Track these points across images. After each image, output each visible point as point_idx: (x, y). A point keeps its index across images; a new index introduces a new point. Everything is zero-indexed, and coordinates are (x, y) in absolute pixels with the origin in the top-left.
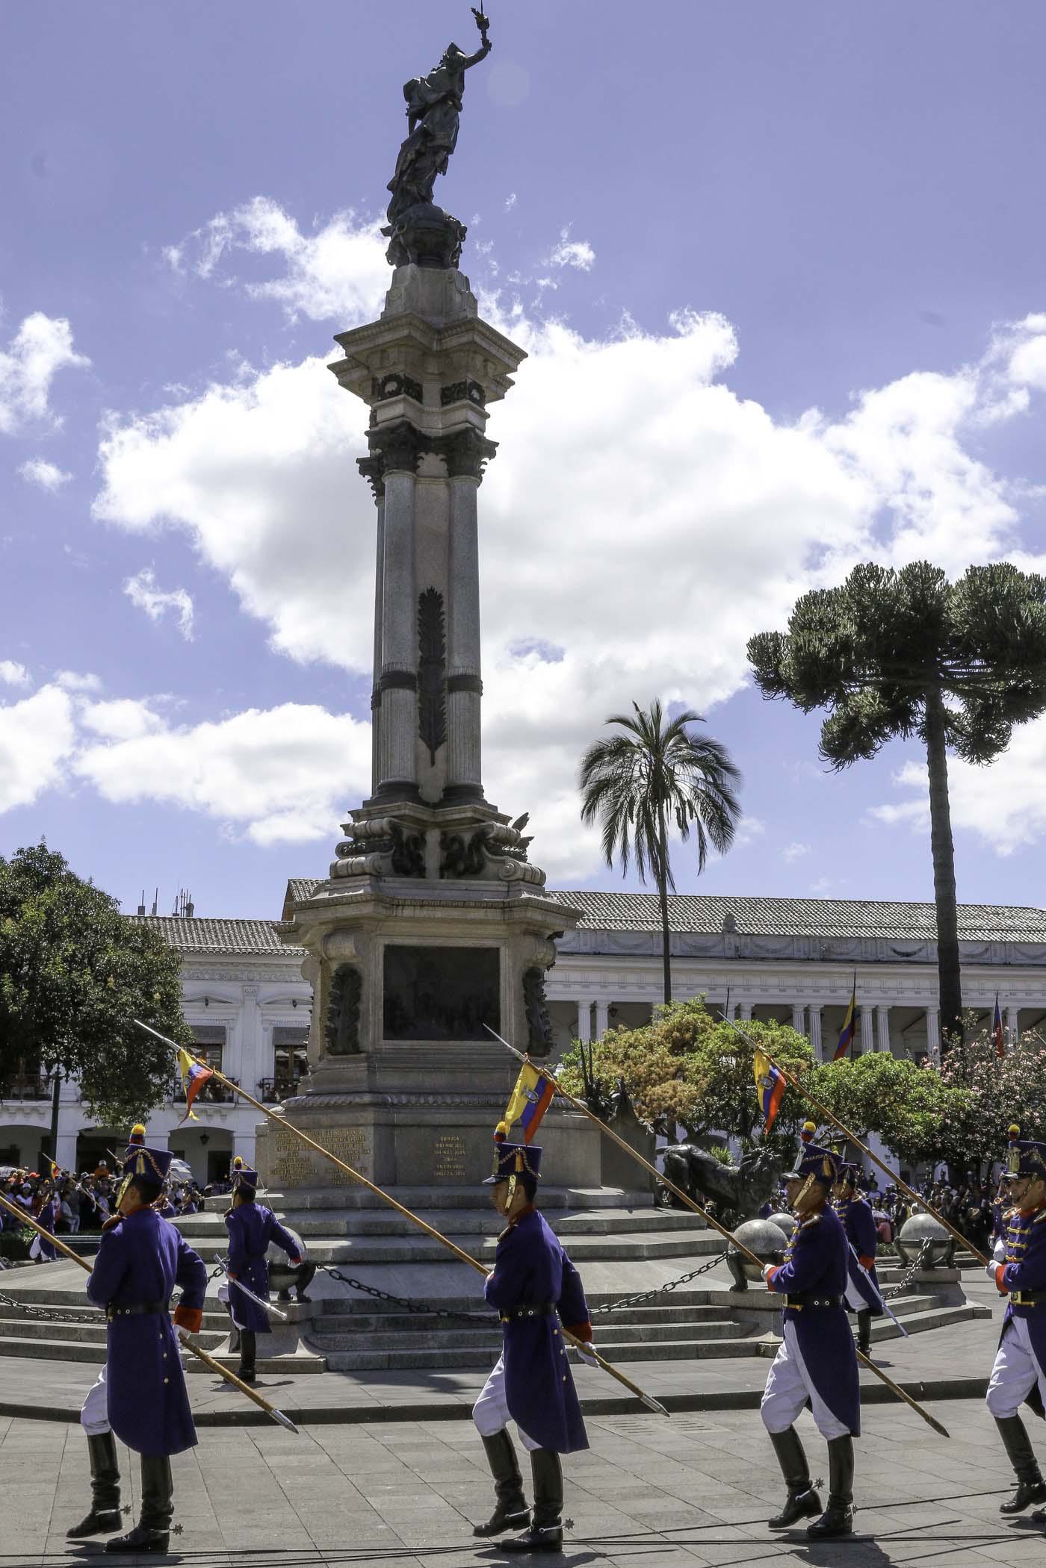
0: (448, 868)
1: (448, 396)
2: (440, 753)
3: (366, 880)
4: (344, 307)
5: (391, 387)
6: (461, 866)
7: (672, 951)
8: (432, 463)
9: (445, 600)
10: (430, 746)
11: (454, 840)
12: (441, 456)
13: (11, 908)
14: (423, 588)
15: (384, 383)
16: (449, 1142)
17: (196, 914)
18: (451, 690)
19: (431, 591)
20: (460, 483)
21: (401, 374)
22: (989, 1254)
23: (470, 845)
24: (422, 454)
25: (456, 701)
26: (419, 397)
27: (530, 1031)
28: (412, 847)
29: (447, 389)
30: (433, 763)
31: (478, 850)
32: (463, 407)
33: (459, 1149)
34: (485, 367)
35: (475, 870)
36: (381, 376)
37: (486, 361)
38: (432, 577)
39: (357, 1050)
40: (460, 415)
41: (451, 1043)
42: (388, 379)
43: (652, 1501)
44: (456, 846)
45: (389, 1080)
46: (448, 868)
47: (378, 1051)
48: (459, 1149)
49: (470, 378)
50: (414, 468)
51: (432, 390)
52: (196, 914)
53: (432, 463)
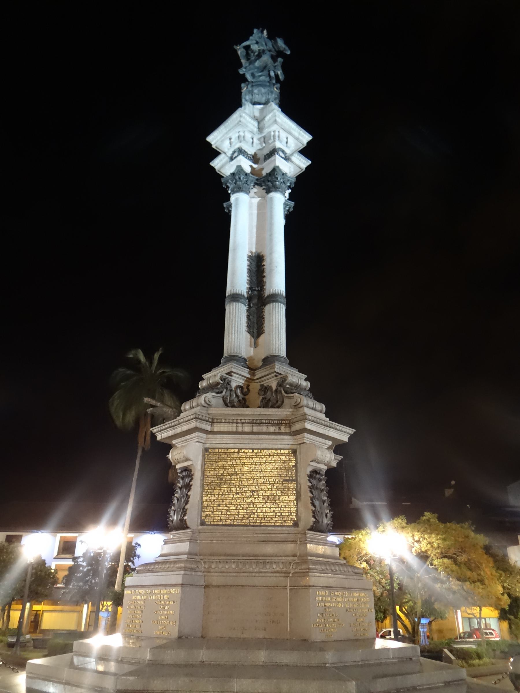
0: (266, 404)
5: (236, 154)
35: (277, 405)
39: (187, 528)
42: (234, 152)
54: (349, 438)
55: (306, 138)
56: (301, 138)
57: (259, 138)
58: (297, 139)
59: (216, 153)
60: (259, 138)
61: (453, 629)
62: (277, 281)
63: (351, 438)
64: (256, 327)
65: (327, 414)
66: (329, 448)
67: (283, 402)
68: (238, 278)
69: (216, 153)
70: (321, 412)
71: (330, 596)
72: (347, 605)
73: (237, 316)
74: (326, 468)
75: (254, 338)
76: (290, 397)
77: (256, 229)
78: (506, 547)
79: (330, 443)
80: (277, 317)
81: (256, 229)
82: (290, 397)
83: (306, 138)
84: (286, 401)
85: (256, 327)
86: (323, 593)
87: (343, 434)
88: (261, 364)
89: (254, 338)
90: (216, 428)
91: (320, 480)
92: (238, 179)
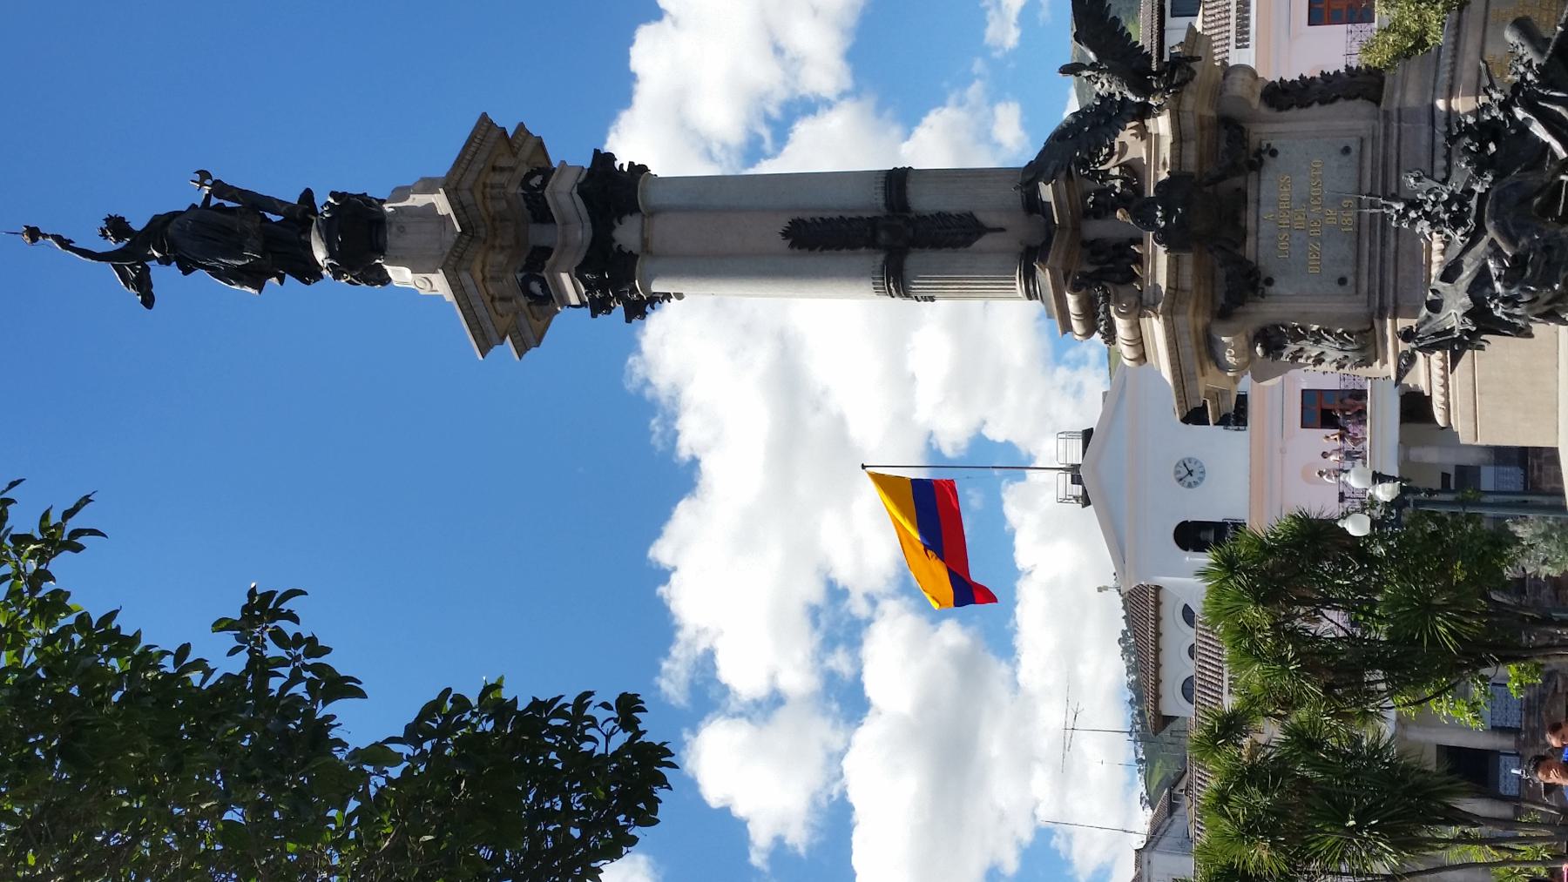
1: (540, 212)
3: (1145, 322)
4: (932, 449)
5: (536, 287)
8: (627, 234)
9: (796, 215)
12: (616, 222)
13: (8, 637)
15: (531, 295)
17: (138, 223)
19: (786, 234)
20: (649, 197)
21: (520, 276)
24: (615, 246)
25: (923, 201)
26: (547, 251)
27: (1348, 98)
28: (1102, 258)
29: (534, 215)
32: (553, 194)
34: (502, 169)
36: (523, 301)
37: (494, 169)
38: (770, 232)
40: (562, 196)
42: (527, 291)
43: (1476, 812)
49: (515, 189)
50: (633, 257)
51: (539, 235)
52: (138, 223)
53: (627, 234)
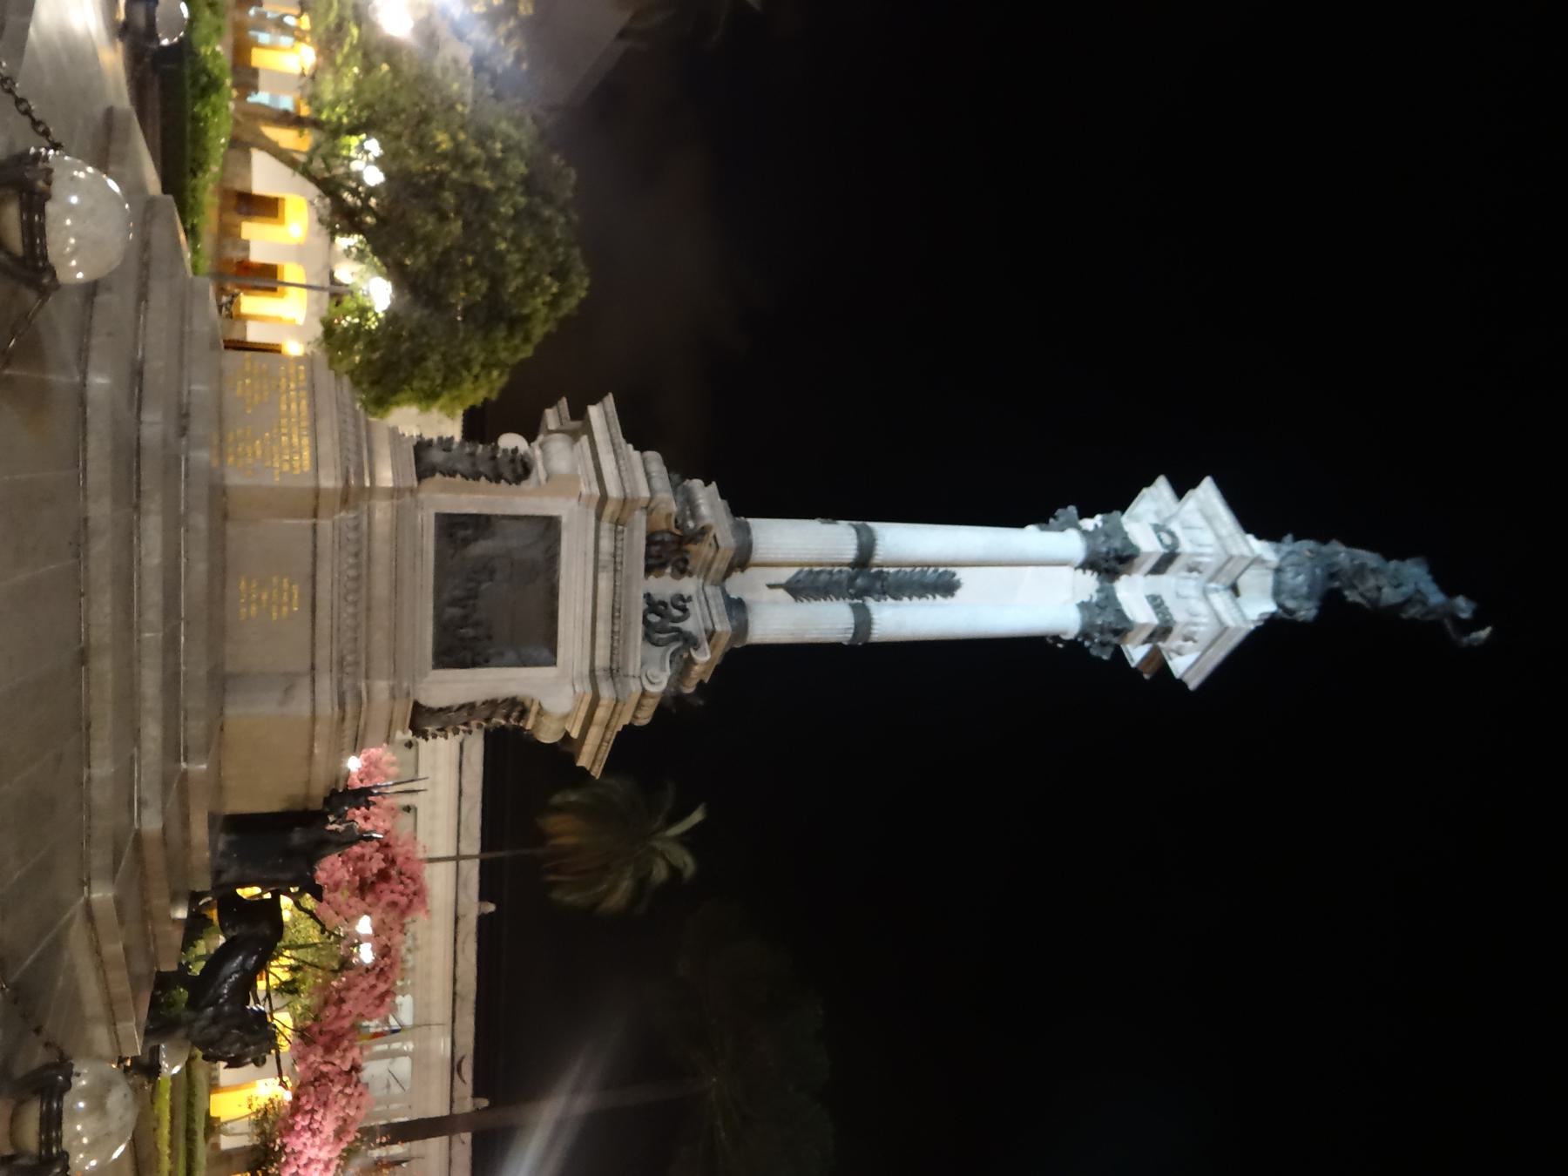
0: (653, 605)
2: (781, 593)
5: (1167, 540)
6: (654, 618)
7: (462, 863)
10: (789, 582)
11: (684, 610)
14: (962, 574)
16: (291, 596)
18: (853, 607)
22: (38, 154)
23: (678, 630)
30: (771, 586)
31: (675, 639)
33: (279, 611)
39: (421, 476)
41: (431, 605)
42: (1172, 534)
44: (677, 613)
45: (382, 511)
46: (653, 605)
47: (418, 505)
48: (279, 611)
54: (583, 768)
55: (1161, 489)
56: (1229, 542)
57: (1195, 575)
58: (1218, 537)
59: (1180, 491)
60: (1195, 575)
61: (335, 490)
62: (897, 619)
63: (584, 772)
64: (808, 585)
65: (629, 729)
66: (567, 736)
67: (656, 644)
68: (906, 542)
69: (1180, 491)
70: (635, 717)
71: (298, 389)
72: (284, 421)
73: (832, 540)
74: (529, 727)
75: (791, 580)
76: (663, 657)
77: (1012, 582)
78: (1085, 634)
79: (575, 734)
80: (828, 621)
81: (1012, 582)
82: (663, 657)
83: (1161, 489)
84: (657, 652)
85: (808, 585)
86: (302, 377)
87: (591, 757)
88: (734, 596)
89: (791, 580)
90: (606, 526)
91: (507, 717)
92: (378, 992)
